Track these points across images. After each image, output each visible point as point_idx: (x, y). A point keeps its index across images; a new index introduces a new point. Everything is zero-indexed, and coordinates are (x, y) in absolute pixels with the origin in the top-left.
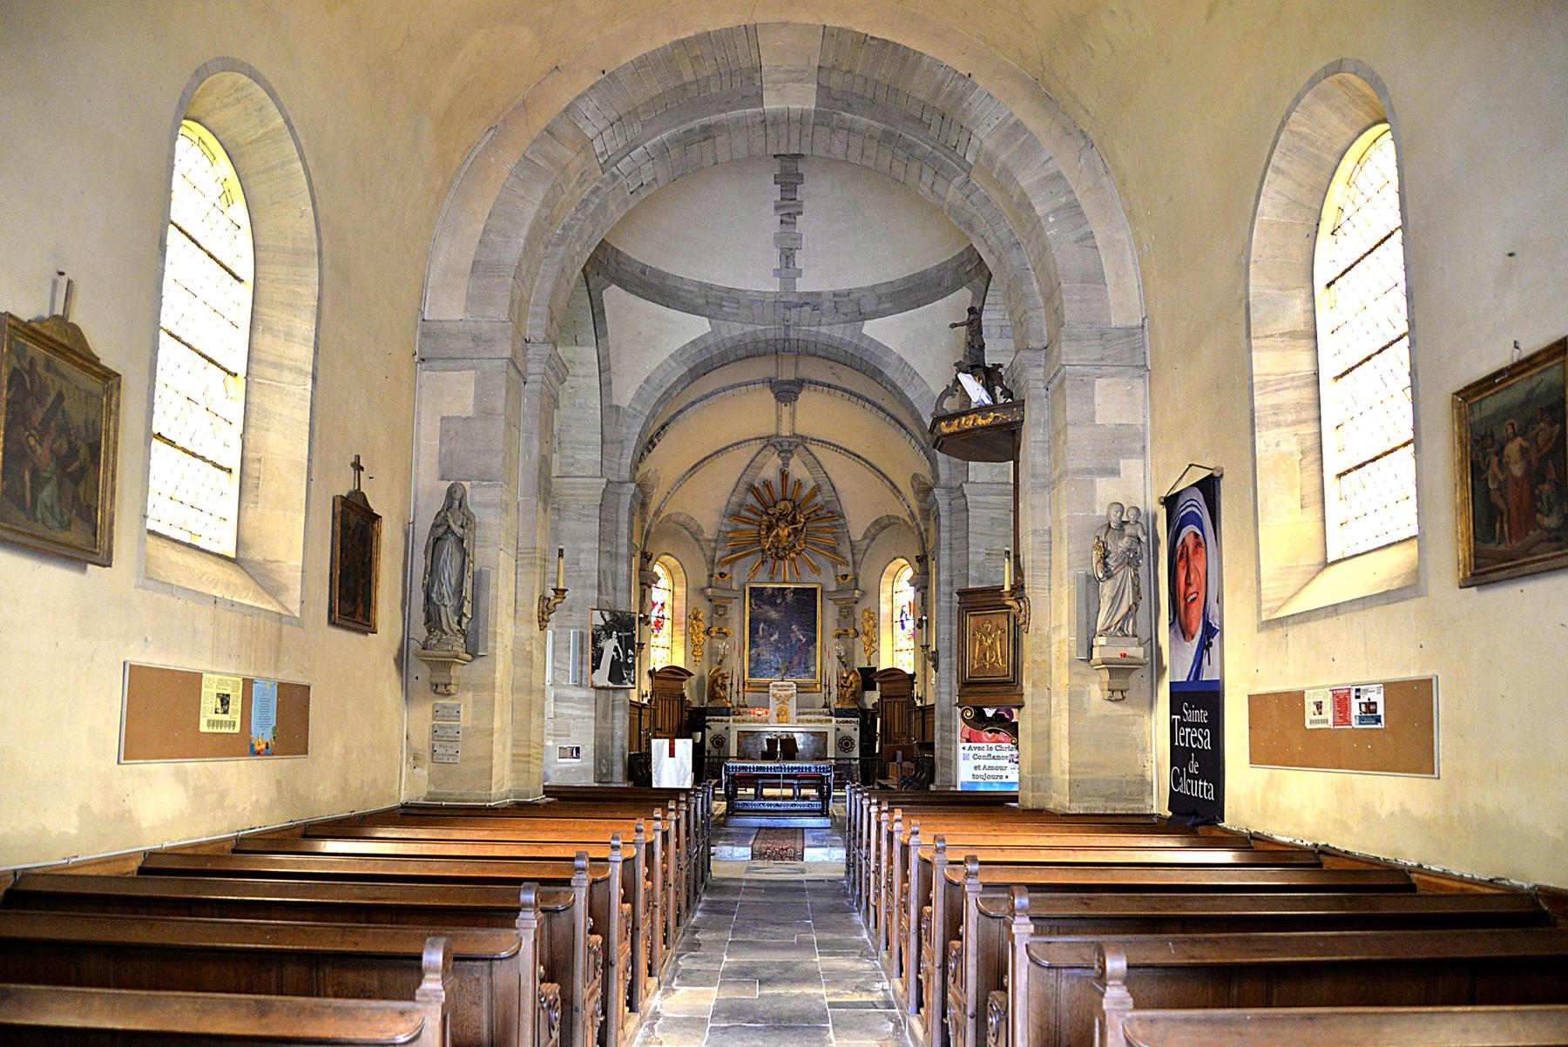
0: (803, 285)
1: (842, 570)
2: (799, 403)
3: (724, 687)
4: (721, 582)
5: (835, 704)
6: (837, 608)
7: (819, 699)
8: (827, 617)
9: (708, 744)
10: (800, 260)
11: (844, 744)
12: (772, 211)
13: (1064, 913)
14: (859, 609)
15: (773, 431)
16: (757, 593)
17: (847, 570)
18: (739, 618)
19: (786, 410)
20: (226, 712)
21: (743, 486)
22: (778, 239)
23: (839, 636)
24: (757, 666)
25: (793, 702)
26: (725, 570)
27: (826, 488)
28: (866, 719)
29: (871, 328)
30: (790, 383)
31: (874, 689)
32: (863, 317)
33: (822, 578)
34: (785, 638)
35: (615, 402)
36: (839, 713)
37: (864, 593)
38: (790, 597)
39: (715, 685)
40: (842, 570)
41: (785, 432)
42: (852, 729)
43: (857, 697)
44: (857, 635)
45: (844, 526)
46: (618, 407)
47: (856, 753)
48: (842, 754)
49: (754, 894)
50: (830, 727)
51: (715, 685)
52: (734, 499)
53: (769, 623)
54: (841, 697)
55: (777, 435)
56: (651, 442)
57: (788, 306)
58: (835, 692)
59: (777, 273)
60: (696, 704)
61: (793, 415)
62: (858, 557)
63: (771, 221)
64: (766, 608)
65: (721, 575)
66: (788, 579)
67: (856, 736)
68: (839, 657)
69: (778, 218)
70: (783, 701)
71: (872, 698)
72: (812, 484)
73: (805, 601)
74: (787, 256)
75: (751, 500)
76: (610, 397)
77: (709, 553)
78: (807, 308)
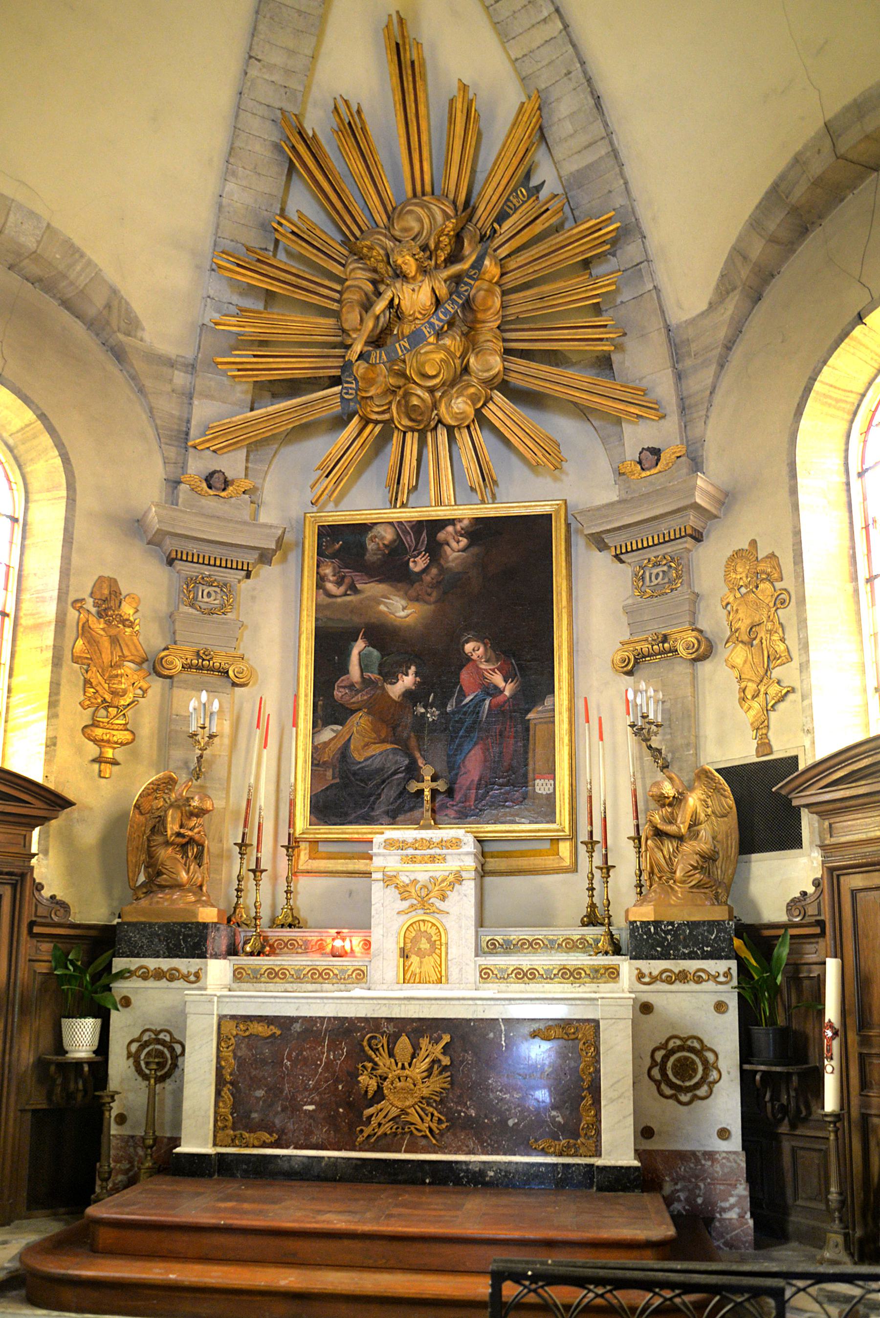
1: (637, 436)
3: (191, 847)
4: (210, 503)
5: (629, 907)
6: (625, 572)
7: (569, 894)
8: (594, 610)
9: (119, 1066)
11: (674, 1068)
13: (516, 1235)
14: (710, 564)
16: (344, 547)
17: (664, 432)
18: (275, 630)
20: (793, 1147)
21: (260, 138)
23: (632, 666)
24: (347, 795)
25: (462, 905)
26: (233, 465)
27: (567, 106)
28: (769, 972)
31: (793, 841)
33: (566, 479)
34: (442, 672)
36: (651, 942)
37: (727, 499)
38: (455, 549)
39: (157, 838)
40: (637, 436)
42: (705, 1005)
43: (715, 876)
44: (704, 652)
45: (638, 270)
47: (726, 1105)
48: (664, 1111)
50: (612, 999)
51: (157, 838)
52: (240, 196)
53: (381, 635)
54: (648, 880)
58: (626, 862)
60: (93, 911)
62: (700, 381)
64: (372, 589)
65: (216, 481)
66: (446, 494)
67: (724, 1036)
68: (642, 731)
70: (424, 898)
71: (781, 881)
72: (504, 105)
73: (508, 580)
75: (302, 204)
77: (168, 407)
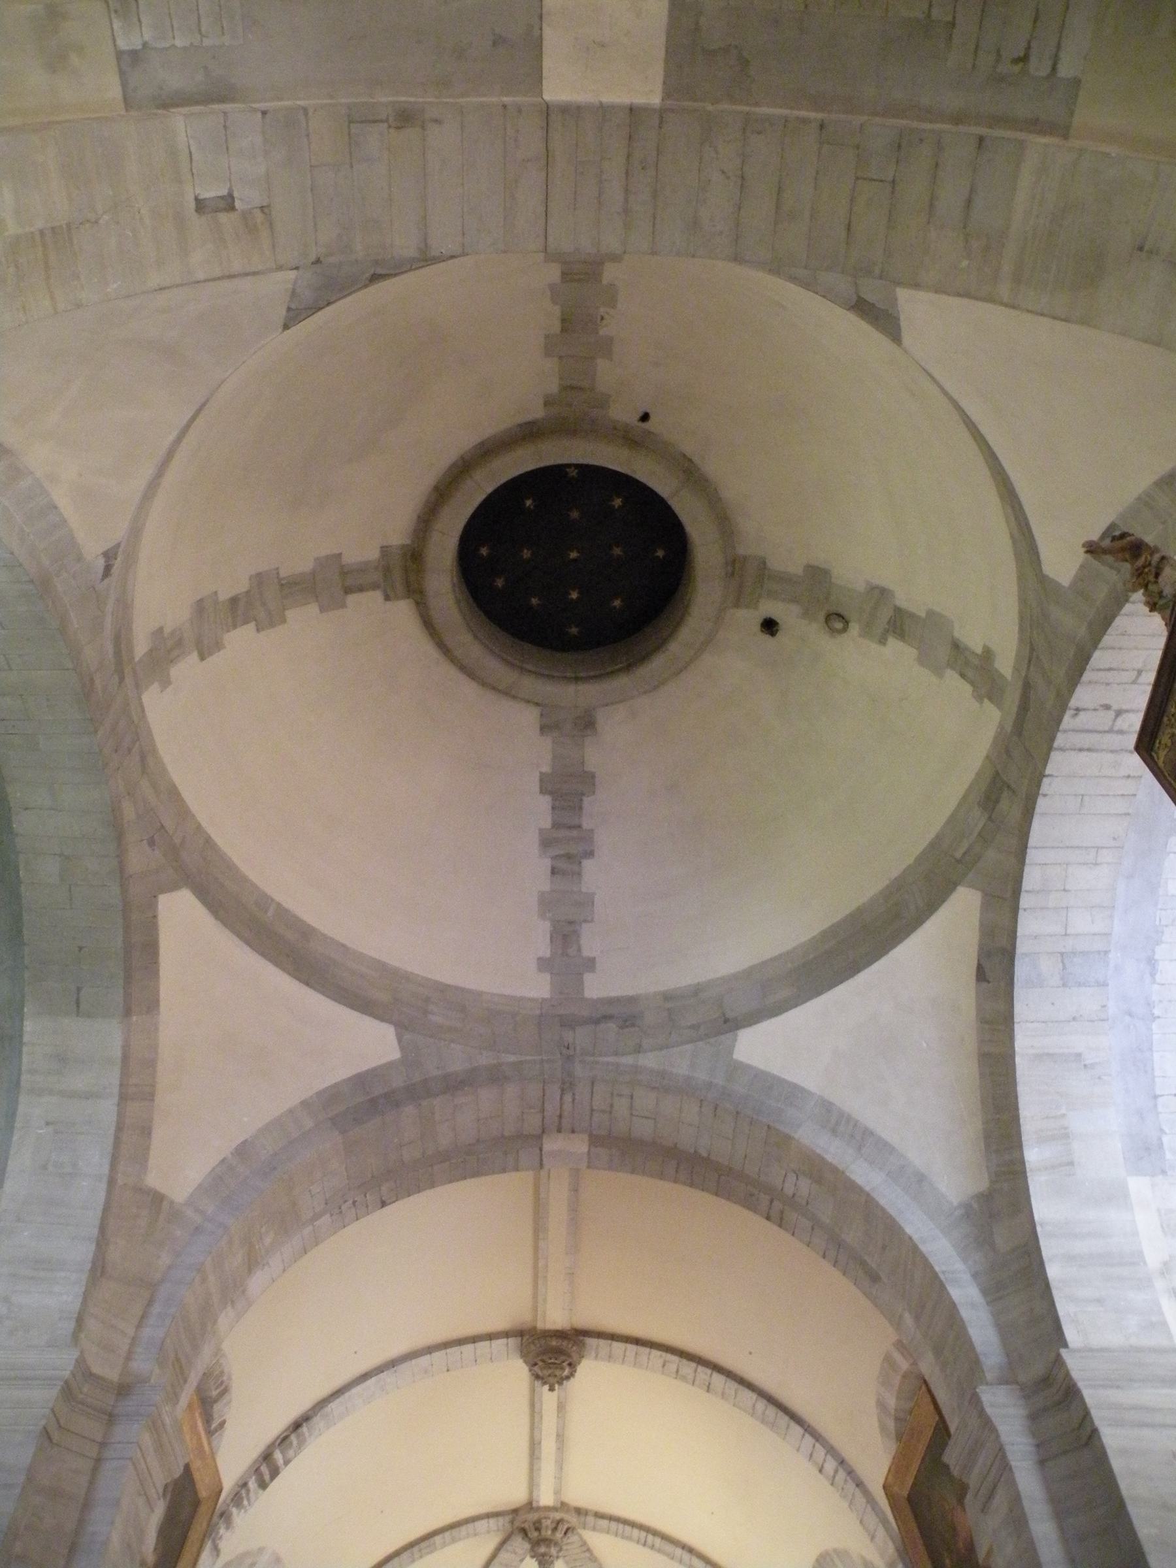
0: (596, 987)
2: (573, 1385)
10: (590, 943)
12: (535, 849)
15: (517, 1495)
19: (549, 1399)
22: (546, 903)
29: (756, 1047)
30: (561, 1334)
32: (731, 1024)
35: (153, 1180)
41: (546, 1498)
46: (157, 1199)
49: (994, 1291)
55: (530, 1506)
56: (267, 1457)
57: (569, 1023)
59: (544, 964)
61: (561, 1407)
63: (534, 872)
69: (547, 863)
74: (565, 935)
76: (141, 1158)
78: (612, 1026)
